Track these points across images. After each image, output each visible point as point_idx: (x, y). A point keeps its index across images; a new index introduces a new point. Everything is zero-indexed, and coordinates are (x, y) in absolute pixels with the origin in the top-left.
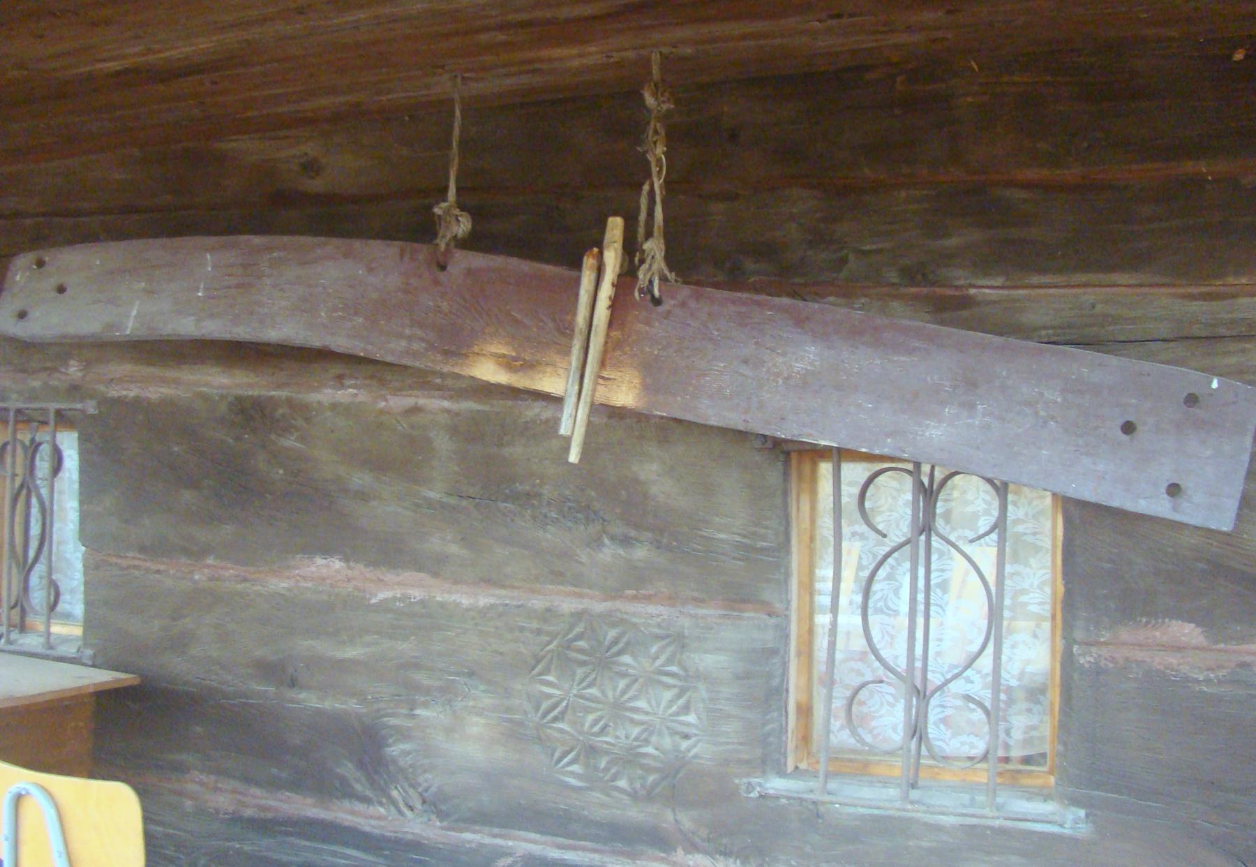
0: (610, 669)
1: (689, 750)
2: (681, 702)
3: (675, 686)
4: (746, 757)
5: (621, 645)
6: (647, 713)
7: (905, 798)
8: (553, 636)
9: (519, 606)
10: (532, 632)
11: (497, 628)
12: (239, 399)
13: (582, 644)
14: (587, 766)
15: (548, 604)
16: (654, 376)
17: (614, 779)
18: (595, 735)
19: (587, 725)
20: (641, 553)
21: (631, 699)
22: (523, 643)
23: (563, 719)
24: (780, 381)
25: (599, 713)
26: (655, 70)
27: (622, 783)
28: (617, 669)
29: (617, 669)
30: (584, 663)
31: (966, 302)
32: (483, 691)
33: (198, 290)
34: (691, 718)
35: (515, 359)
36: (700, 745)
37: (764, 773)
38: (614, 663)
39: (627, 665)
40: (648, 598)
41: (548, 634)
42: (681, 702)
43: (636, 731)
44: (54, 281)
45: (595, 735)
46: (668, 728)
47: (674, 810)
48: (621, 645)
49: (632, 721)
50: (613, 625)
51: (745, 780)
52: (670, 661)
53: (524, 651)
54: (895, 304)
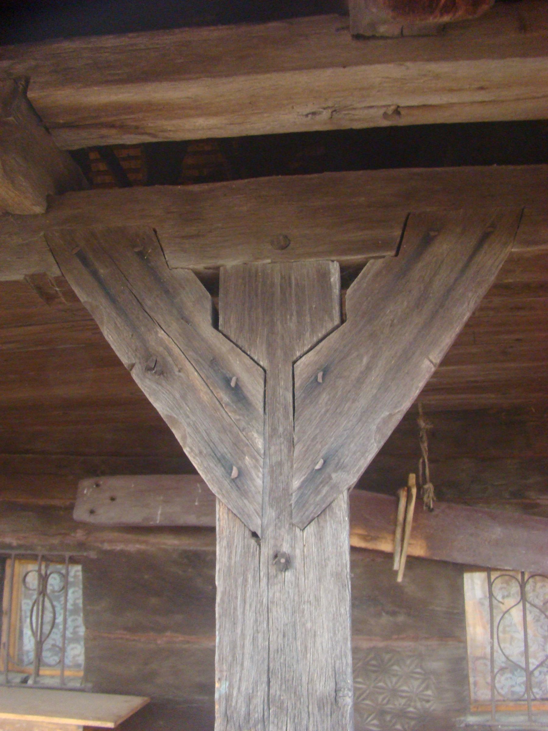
1: (430, 707)
6: (407, 692)
7: (530, 720)
12: (185, 551)
13: (374, 662)
16: (431, 540)
17: (394, 725)
18: (384, 705)
20: (401, 618)
24: (487, 543)
26: (420, 410)
30: (374, 672)
31: (537, 506)
33: (195, 501)
34: (429, 692)
35: (368, 536)
39: (396, 671)
40: (403, 639)
42: (424, 685)
43: (403, 701)
44: (108, 494)
48: (392, 662)
54: (507, 506)
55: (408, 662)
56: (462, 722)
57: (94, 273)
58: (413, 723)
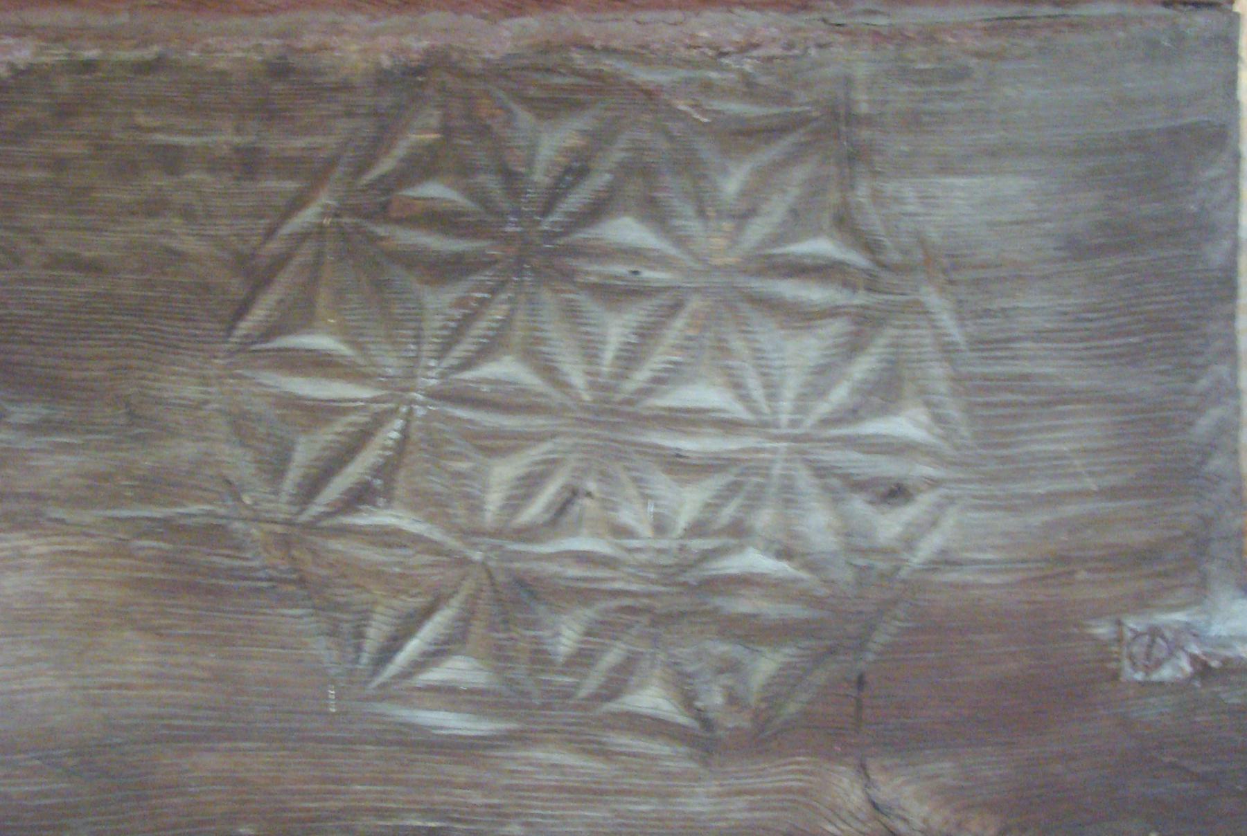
0: (568, 276)
1: (909, 543)
2: (863, 367)
3: (832, 312)
4: (1138, 537)
5: (600, 180)
6: (729, 426)
8: (315, 172)
9: (143, 68)
10: (214, 164)
11: (59, 164)
13: (436, 191)
14: (499, 656)
15: (273, 45)
17: (615, 686)
18: (528, 534)
19: (494, 501)
21: (659, 381)
22: (187, 214)
23: (388, 494)
25: (537, 452)
27: (651, 698)
28: (594, 270)
29: (594, 270)
30: (444, 270)
32: (33, 428)
34: (907, 424)
36: (951, 520)
37: (1201, 591)
38: (576, 251)
39: (633, 254)
41: (288, 166)
42: (863, 367)
43: (688, 501)
45: (528, 534)
46: (821, 471)
47: (862, 768)
48: (600, 180)
49: (678, 465)
50: (554, 105)
51: (1133, 623)
52: (799, 220)
53: (189, 244)
55: (732, 183)
56: (1175, 648)
57: (81, 476)
58: (766, 665)
